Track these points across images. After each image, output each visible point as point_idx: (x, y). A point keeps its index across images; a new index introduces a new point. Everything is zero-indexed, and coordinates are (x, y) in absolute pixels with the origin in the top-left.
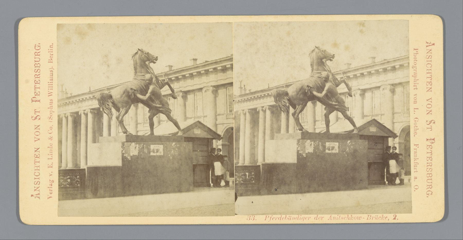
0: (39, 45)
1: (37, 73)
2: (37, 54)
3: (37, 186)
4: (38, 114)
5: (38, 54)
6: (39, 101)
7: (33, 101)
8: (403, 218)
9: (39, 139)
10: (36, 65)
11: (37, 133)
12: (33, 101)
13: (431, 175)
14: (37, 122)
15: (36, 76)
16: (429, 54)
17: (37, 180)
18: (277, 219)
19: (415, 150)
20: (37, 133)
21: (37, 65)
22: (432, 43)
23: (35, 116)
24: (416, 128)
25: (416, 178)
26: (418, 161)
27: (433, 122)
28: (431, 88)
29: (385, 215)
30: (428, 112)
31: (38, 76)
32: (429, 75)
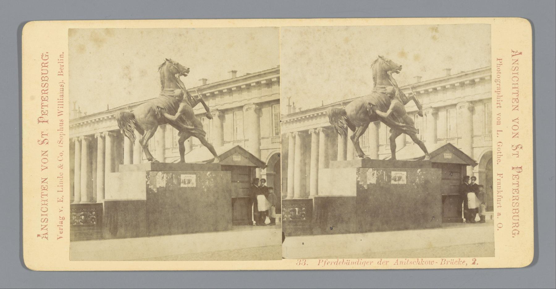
0: (47, 54)
1: (45, 88)
2: (45, 65)
3: (45, 224)
4: (45, 137)
5: (46, 65)
6: (47, 122)
7: (39, 122)
8: (484, 262)
9: (47, 168)
10: (43, 79)
11: (45, 161)
12: (39, 122)
13: (517, 211)
14: (44, 147)
15: (43, 92)
16: (515, 65)
17: (44, 217)
18: (333, 264)
19: (499, 181)
20: (45, 161)
21: (44, 78)
22: (519, 51)
23: (42, 139)
24: (499, 154)
25: (499, 214)
26: (501, 194)
27: (520, 146)
28: (517, 106)
29: (462, 259)
30: (514, 134)
31: (46, 92)
32: (515, 91)
